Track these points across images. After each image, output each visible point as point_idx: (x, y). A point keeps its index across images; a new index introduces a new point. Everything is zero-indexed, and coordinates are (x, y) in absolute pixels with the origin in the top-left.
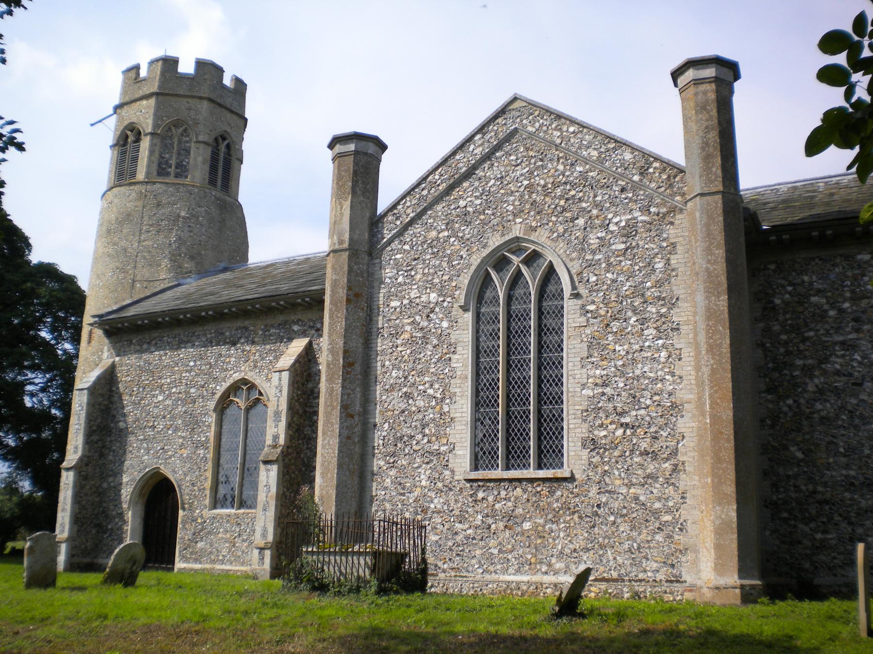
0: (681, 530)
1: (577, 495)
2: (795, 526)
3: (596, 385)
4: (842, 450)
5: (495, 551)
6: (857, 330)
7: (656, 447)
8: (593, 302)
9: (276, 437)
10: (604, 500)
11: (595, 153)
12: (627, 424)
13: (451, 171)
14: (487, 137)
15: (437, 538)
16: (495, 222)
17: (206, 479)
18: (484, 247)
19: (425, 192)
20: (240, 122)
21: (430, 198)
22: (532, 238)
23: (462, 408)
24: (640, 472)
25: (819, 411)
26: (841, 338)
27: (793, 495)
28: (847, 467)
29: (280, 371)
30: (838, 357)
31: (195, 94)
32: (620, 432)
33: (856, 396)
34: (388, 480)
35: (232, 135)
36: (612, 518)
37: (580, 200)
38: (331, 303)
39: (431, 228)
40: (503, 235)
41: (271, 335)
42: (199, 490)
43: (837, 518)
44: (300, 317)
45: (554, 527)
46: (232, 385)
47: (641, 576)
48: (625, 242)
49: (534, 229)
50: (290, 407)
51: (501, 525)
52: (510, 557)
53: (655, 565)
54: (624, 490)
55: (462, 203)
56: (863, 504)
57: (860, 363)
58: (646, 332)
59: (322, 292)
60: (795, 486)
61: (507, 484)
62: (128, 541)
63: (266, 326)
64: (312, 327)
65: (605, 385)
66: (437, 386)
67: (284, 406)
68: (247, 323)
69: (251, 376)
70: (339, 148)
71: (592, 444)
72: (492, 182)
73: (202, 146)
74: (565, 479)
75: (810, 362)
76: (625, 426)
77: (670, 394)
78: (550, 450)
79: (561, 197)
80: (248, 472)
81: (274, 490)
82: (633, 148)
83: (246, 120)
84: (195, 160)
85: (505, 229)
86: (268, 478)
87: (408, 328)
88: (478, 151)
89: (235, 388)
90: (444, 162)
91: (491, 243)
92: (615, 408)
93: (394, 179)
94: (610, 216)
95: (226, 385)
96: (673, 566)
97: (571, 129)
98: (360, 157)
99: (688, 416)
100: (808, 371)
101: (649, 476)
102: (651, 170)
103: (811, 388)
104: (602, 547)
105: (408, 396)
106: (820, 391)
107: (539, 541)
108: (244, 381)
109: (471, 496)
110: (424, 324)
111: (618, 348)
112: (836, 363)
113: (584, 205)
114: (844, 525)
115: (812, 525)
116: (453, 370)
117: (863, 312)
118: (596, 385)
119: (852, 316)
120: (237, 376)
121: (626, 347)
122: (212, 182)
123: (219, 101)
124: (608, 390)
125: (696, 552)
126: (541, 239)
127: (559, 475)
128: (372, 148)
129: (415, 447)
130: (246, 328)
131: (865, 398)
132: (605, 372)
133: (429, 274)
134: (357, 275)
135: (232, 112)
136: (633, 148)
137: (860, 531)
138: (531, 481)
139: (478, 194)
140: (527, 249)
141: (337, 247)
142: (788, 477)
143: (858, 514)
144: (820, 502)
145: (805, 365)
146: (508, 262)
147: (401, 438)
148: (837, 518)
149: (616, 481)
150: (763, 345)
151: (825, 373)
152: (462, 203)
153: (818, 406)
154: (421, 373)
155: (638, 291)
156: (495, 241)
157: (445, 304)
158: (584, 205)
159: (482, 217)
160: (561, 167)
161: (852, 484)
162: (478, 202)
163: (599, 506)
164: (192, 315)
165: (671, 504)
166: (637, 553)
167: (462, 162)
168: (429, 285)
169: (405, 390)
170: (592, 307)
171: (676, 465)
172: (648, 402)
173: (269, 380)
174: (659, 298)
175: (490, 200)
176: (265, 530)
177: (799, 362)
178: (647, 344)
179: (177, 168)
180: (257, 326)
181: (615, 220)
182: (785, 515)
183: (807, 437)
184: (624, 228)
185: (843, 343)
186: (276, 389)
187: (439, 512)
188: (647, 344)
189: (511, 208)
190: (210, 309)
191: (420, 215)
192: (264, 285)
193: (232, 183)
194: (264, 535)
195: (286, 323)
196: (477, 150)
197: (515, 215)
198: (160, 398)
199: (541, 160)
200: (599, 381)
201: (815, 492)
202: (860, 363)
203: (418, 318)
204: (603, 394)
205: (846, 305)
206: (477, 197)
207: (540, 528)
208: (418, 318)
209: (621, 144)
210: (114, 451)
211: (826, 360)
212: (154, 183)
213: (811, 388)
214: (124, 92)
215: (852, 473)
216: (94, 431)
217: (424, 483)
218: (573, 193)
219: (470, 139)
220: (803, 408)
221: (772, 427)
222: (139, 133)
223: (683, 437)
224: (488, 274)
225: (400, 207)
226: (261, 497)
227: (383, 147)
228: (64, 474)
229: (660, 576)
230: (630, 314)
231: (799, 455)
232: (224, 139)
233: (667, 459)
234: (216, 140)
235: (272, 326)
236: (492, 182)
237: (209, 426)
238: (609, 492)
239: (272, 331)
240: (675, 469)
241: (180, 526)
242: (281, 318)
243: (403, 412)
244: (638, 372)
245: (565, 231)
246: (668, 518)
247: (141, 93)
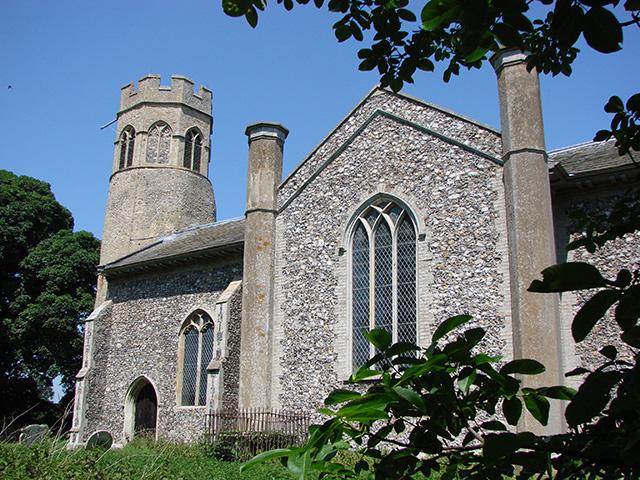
13: (333, 146)
14: (358, 118)
19: (314, 163)
21: (318, 167)
29: (221, 303)
34: (291, 383)
39: (317, 190)
40: (370, 192)
55: (341, 170)
62: (414, 420)
68: (201, 268)
84: (174, 149)
87: (303, 267)
88: (351, 129)
91: (361, 199)
94: (448, 173)
95: (187, 314)
113: (429, 166)
120: (195, 308)
122: (187, 164)
130: (201, 272)
132: (445, 295)
139: (352, 162)
154: (312, 301)
156: (365, 197)
157: (330, 247)
159: (355, 179)
167: (340, 138)
168: (318, 233)
170: (435, 245)
172: (479, 317)
175: (362, 165)
181: (452, 176)
189: (375, 171)
191: (310, 181)
196: (351, 128)
198: (144, 325)
208: (310, 258)
217: (316, 385)
218: (421, 157)
223: (505, 343)
232: (195, 133)
234: (188, 133)
235: (219, 270)
239: (219, 273)
241: (158, 418)
245: (415, 187)
247: (134, 103)
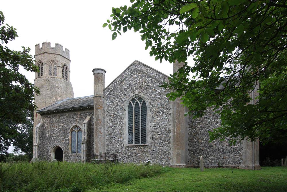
0: (170, 155)
1: (149, 149)
2: (194, 155)
3: (153, 126)
4: (205, 140)
5: (133, 160)
6: (210, 115)
7: (165, 139)
8: (153, 109)
9: (84, 138)
10: (155, 149)
11: (154, 75)
12: (159, 134)
15: (121, 158)
16: (131, 91)
17: (69, 147)
18: (129, 96)
19: (115, 83)
20: (69, 61)
22: (140, 94)
23: (126, 131)
24: (162, 144)
25: (200, 132)
26: (206, 116)
27: (194, 148)
28: (206, 143)
30: (205, 120)
31: (56, 53)
32: (158, 136)
33: (208, 128)
35: (67, 65)
36: (156, 153)
37: (150, 86)
38: (95, 108)
39: (117, 92)
40: (133, 94)
41: (82, 115)
42: (68, 150)
43: (203, 153)
44: (88, 111)
45: (145, 155)
46: (73, 127)
47: (162, 164)
48: (160, 96)
49: (140, 92)
50: (87, 132)
51: (134, 155)
52: (136, 161)
53: (165, 162)
54: (159, 147)
55: (124, 86)
56: (209, 150)
57: (210, 122)
58: (164, 115)
59: (93, 106)
60: (195, 147)
61: (135, 147)
63: (80, 113)
64: (91, 114)
65: (155, 126)
66: (120, 127)
67: (86, 131)
68: (76, 113)
69: (78, 125)
70: (95, 72)
71: (152, 139)
72: (131, 81)
73: (60, 68)
74: (147, 145)
75: (199, 121)
76: (159, 135)
77: (168, 128)
78: (144, 140)
79: (146, 85)
80: (79, 147)
81: (85, 149)
82: (162, 74)
83: (70, 61)
85: (134, 92)
86: (84, 147)
87: (113, 114)
89: (74, 127)
90: (120, 76)
92: (157, 131)
93: (108, 80)
94: (157, 90)
95: (72, 127)
96: (168, 162)
97: (149, 69)
98: (98, 74)
99: (172, 133)
100: (199, 123)
101: (163, 145)
102: (166, 79)
103: (199, 127)
104: (154, 159)
105: (113, 129)
106: (201, 128)
107: (141, 158)
108: (76, 126)
109: (127, 149)
110: (116, 113)
111: (158, 119)
112: (205, 122)
113: (151, 87)
114: (204, 154)
115: (198, 154)
116: (123, 123)
117: (211, 111)
118: (153, 126)
119: (209, 112)
120: (74, 125)
121: (159, 118)
122: (63, 77)
123: (63, 55)
124: (155, 127)
125: (173, 159)
126: (142, 94)
127: (146, 145)
128: (103, 72)
129: (115, 140)
131: (210, 129)
133: (117, 102)
134: (101, 102)
135: (66, 58)
136: (162, 74)
137: (208, 156)
138: (140, 146)
140: (139, 97)
141: (96, 96)
142: (193, 145)
143: (207, 152)
144: (199, 150)
145: (198, 122)
146: (135, 100)
147: (113, 137)
148: (203, 153)
149: (157, 146)
150: (189, 118)
151: (202, 124)
152: (124, 86)
153: (200, 131)
155: (162, 107)
157: (121, 109)
158: (151, 87)
159: (129, 89)
160: (146, 78)
161: (206, 146)
162: (128, 86)
163: (153, 151)
164: (57, 111)
165: (168, 150)
166: (161, 160)
168: (117, 105)
169: (113, 128)
170: (153, 110)
171: (169, 142)
172: (164, 130)
173: (82, 125)
174: (167, 108)
176: (83, 157)
177: (197, 122)
178: (164, 118)
179: (54, 73)
180: (78, 114)
181: (158, 91)
182: (192, 152)
183: (198, 137)
184: (160, 92)
185: (206, 117)
186: (84, 127)
187: (121, 152)
188: (164, 118)
190: (67, 109)
192: (79, 104)
193: (68, 78)
194: (83, 159)
195: (85, 113)
197: (136, 89)
198: (56, 130)
199: (142, 76)
200: (154, 126)
201: (199, 148)
202: (210, 122)
203: (115, 112)
204: (155, 128)
205: (208, 109)
206: (128, 85)
207: (142, 155)
209: (160, 73)
210: (46, 142)
211: (203, 121)
212: (48, 77)
213: (199, 127)
214: (36, 52)
215: (206, 144)
216: (41, 137)
217: (117, 147)
219: (125, 71)
220: (197, 131)
221: (190, 135)
222: (42, 63)
224: (130, 103)
225: (110, 86)
226: (82, 151)
227: (105, 72)
228: (34, 148)
229: (166, 164)
230: (160, 111)
231: (196, 141)
232: (65, 66)
233: (167, 141)
234: (63, 66)
235: (82, 113)
236: (131, 81)
237: (69, 136)
238: (156, 148)
239: (82, 114)
240: (169, 143)
242: (84, 112)
243: (112, 132)
244: (162, 124)
246: (168, 153)
247: (41, 52)
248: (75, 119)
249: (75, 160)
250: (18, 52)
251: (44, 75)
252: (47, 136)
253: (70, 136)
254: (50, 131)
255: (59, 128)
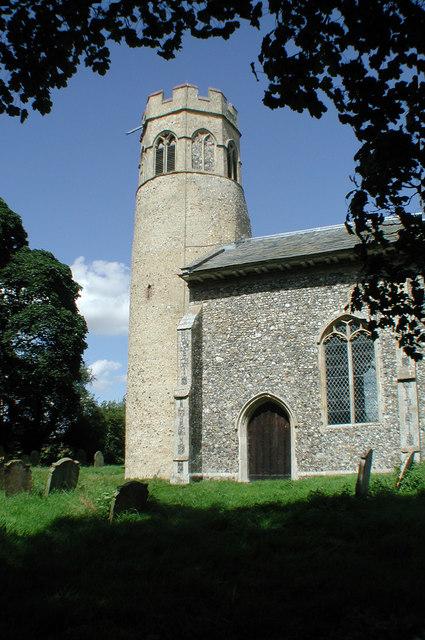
42: (313, 410)
83: (241, 135)
95: (328, 322)
194: (410, 442)
198: (259, 335)
248: (341, 293)
249: (347, 450)
250: (356, 123)
251: (179, 166)
252: (219, 359)
253: (319, 355)
254: (229, 340)
255: (272, 328)
